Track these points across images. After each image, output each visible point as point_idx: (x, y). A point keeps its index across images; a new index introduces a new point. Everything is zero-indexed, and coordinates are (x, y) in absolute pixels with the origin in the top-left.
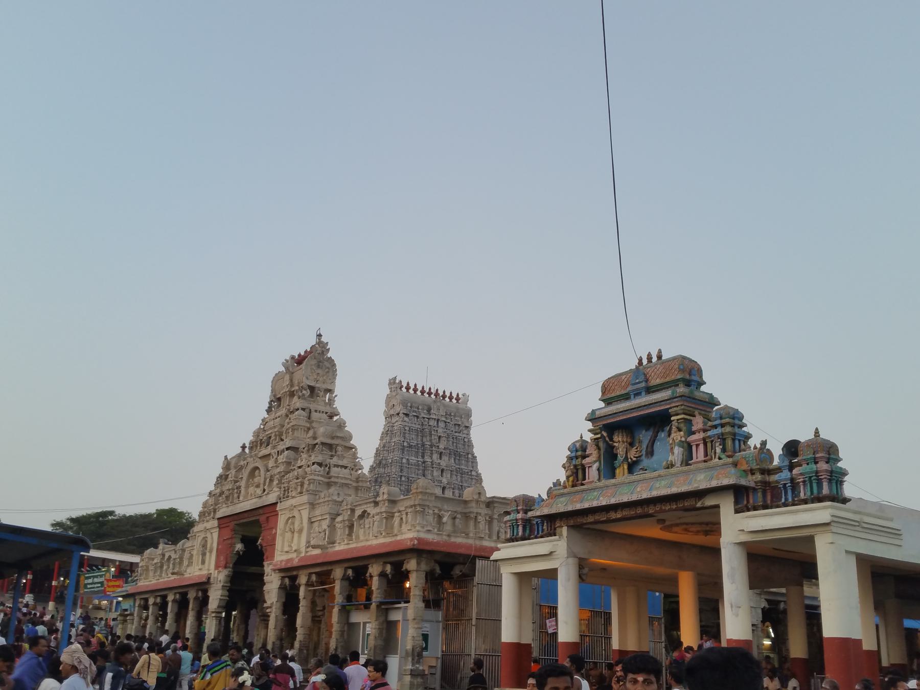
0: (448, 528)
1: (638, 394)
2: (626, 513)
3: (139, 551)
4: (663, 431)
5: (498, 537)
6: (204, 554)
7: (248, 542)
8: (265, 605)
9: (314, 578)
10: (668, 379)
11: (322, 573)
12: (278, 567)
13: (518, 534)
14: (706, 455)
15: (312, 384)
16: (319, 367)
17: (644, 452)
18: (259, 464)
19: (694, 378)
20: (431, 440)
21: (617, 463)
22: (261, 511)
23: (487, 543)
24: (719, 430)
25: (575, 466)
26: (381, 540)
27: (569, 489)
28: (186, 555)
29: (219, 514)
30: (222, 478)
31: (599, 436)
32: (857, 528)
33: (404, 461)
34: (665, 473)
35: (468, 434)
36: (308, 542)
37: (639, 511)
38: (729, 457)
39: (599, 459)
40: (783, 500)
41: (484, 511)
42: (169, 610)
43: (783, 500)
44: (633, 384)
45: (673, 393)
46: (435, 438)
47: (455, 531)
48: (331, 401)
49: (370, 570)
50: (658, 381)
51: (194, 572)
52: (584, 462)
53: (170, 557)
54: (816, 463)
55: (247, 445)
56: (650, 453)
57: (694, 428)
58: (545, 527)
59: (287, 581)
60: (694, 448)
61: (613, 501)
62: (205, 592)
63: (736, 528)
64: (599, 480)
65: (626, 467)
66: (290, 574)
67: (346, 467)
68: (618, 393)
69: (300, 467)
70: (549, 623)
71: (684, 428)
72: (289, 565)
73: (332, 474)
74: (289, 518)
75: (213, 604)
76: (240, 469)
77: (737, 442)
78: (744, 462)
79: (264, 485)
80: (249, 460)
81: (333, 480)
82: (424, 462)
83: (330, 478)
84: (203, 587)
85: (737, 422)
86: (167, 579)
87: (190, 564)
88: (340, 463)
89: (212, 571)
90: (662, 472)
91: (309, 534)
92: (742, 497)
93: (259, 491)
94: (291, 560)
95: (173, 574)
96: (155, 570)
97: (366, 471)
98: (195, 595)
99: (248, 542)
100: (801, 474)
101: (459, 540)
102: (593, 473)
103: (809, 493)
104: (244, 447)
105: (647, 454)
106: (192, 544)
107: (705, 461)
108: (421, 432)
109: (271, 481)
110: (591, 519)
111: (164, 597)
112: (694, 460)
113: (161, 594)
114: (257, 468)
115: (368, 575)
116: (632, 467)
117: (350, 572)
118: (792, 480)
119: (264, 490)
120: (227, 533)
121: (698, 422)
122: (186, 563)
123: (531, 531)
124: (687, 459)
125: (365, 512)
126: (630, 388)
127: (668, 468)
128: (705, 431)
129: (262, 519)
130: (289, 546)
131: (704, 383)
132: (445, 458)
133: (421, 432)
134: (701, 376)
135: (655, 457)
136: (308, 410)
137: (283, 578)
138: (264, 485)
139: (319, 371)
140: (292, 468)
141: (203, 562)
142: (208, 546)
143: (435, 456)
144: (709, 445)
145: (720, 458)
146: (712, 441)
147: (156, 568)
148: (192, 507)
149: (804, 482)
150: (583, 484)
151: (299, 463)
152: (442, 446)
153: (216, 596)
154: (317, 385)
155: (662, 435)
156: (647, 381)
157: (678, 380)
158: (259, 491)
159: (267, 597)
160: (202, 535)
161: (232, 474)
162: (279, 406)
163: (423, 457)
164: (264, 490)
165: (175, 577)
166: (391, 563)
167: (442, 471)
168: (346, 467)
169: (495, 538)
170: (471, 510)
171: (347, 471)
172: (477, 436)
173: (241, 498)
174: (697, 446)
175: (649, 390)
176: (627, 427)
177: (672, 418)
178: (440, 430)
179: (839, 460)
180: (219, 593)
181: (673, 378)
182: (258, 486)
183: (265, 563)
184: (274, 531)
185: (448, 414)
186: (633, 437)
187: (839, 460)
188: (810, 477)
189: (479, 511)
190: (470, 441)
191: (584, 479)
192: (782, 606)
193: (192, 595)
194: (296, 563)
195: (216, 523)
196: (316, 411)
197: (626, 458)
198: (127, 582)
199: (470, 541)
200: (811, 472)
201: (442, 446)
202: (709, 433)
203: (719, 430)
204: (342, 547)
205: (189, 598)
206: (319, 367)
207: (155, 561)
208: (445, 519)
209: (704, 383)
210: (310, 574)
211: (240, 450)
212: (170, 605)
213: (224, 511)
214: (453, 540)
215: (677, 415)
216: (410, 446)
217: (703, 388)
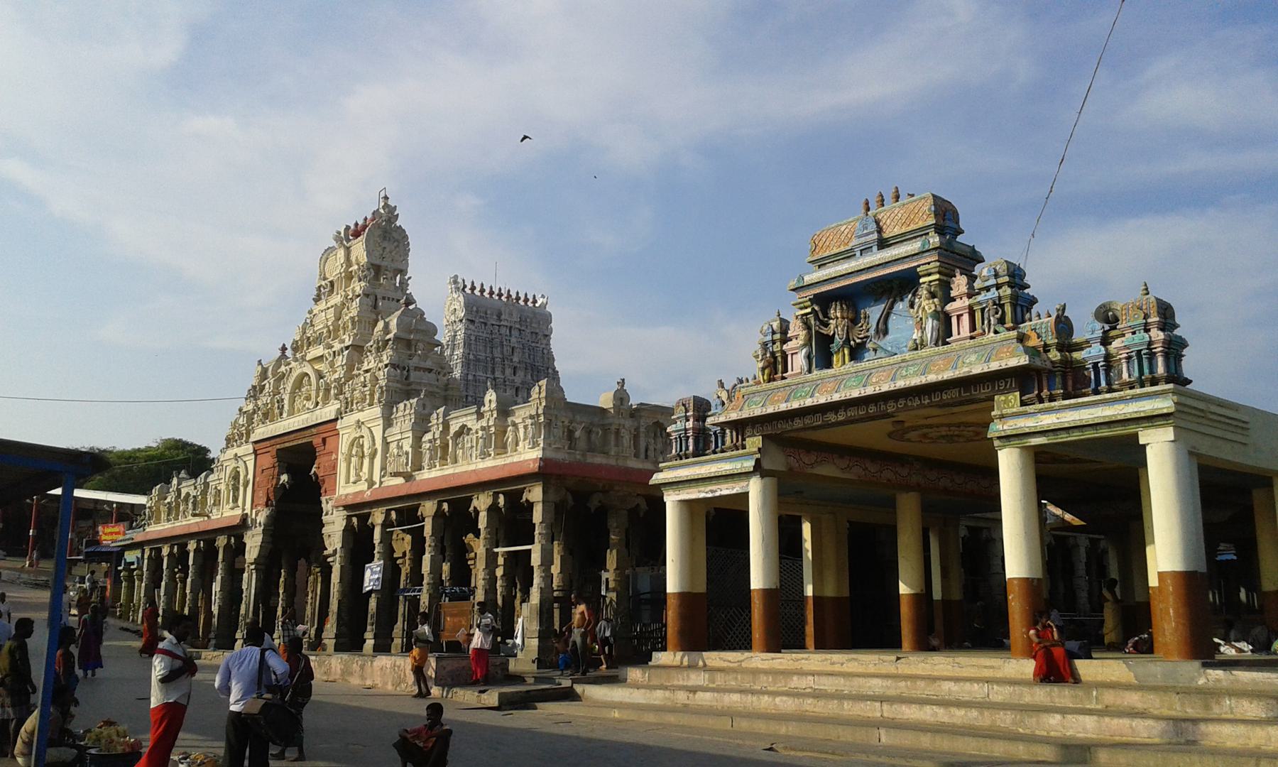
0: (582, 444)
1: (865, 250)
2: (852, 413)
3: (145, 491)
4: (902, 300)
5: (646, 457)
6: (236, 489)
7: (297, 471)
8: (326, 553)
9: (394, 515)
10: (912, 227)
11: (405, 511)
12: (344, 503)
13: (687, 448)
14: (973, 328)
15: (378, 262)
16: (385, 238)
17: (872, 332)
18: (307, 369)
19: (948, 223)
20: (502, 353)
21: (834, 347)
22: (314, 430)
23: (634, 464)
24: (993, 293)
25: (773, 354)
26: (489, 463)
27: (765, 386)
28: (211, 491)
29: (254, 438)
30: (255, 392)
31: (809, 310)
32: (1200, 420)
33: (470, 377)
34: (904, 356)
35: (548, 344)
36: (383, 468)
37: (872, 409)
38: (1008, 329)
39: (808, 343)
40: (1093, 385)
41: (628, 423)
42: (191, 562)
43: (1093, 385)
44: (860, 237)
45: (923, 245)
46: (507, 350)
47: (591, 449)
48: (404, 284)
49: (475, 503)
50: (897, 231)
51: (226, 514)
52: (785, 347)
53: (188, 494)
54: (1147, 331)
55: (288, 346)
56: (883, 330)
57: (953, 294)
58: (728, 439)
59: (355, 520)
60: (954, 320)
61: (836, 397)
62: (240, 538)
63: (1020, 423)
64: (810, 371)
65: (846, 352)
66: (358, 510)
67: (430, 371)
68: (836, 251)
69: (367, 371)
70: (1228, 555)
71: (939, 294)
72: (358, 500)
73: (412, 379)
74: (355, 439)
75: (252, 553)
76: (281, 378)
77: (1019, 309)
78: (1033, 335)
79: (317, 397)
80: (293, 364)
81: (413, 387)
82: (495, 379)
83: (409, 384)
84: (237, 530)
85: (1017, 280)
86: (187, 522)
87: (217, 503)
88: (423, 365)
89: (248, 511)
90: (908, 356)
91: (384, 458)
92: (1028, 381)
93: (310, 405)
94: (362, 492)
95: (194, 515)
96: (168, 518)
97: (457, 373)
98: (489, 501)
99: (297, 471)
100: (1126, 347)
101: (599, 460)
102: (798, 362)
103: (1136, 374)
104: (284, 349)
105: (877, 331)
106: (219, 479)
107: (972, 338)
108: (490, 343)
109: (327, 390)
110: (798, 423)
111: (183, 547)
112: (955, 336)
113: (179, 541)
114: (307, 374)
115: (471, 509)
116: (856, 353)
117: (445, 506)
118: (1108, 357)
119: (317, 404)
120: (268, 460)
121: (960, 284)
122: (210, 500)
123: (707, 446)
124: (944, 334)
125: (464, 426)
126: (855, 242)
127: (916, 349)
128: (970, 296)
129: (317, 441)
130: (348, 482)
131: (962, 232)
132: (520, 374)
133: (490, 343)
134: (957, 222)
135: (888, 337)
136: (372, 297)
137: (349, 518)
138: (317, 397)
139: (385, 244)
140: (355, 372)
141: (235, 499)
142: (242, 477)
143: (508, 371)
144: (978, 315)
145: (996, 332)
146: (983, 310)
147: (170, 509)
148: (209, 436)
149: (1129, 358)
150: (783, 378)
151: (365, 367)
152: (516, 359)
153: (253, 543)
154: (384, 264)
155: (901, 306)
156: (880, 230)
157: (928, 227)
158: (310, 405)
159: (327, 543)
160: (233, 464)
161: (268, 386)
162: (332, 291)
163: (493, 372)
164: (317, 404)
165: (198, 519)
166: (503, 493)
167: (517, 389)
168: (430, 371)
169: (642, 456)
170: (611, 420)
171: (432, 375)
172: (558, 344)
173: (285, 415)
174: (959, 317)
175: (883, 244)
176: (852, 297)
177: (922, 280)
178: (513, 340)
179: (1176, 326)
180: (259, 539)
181: (921, 224)
182: (308, 399)
183: (323, 499)
184: (334, 456)
185: (522, 320)
186: (857, 313)
187: (1176, 326)
188: (1139, 351)
189: (622, 421)
190: (550, 352)
191: (785, 370)
192: (985, 534)
193: (221, 541)
194: (368, 496)
195: (250, 448)
196: (384, 298)
197: (847, 341)
198: (131, 528)
199: (612, 462)
200: (1141, 344)
201: (516, 359)
202: (979, 298)
203: (993, 293)
204: (431, 475)
205: (218, 548)
206: (385, 238)
207: (168, 500)
208: (577, 434)
209: (962, 232)
210: (388, 512)
211: (279, 353)
212: (191, 555)
213: (261, 432)
214: (589, 460)
215: (929, 275)
216: (478, 360)
217: (960, 239)
